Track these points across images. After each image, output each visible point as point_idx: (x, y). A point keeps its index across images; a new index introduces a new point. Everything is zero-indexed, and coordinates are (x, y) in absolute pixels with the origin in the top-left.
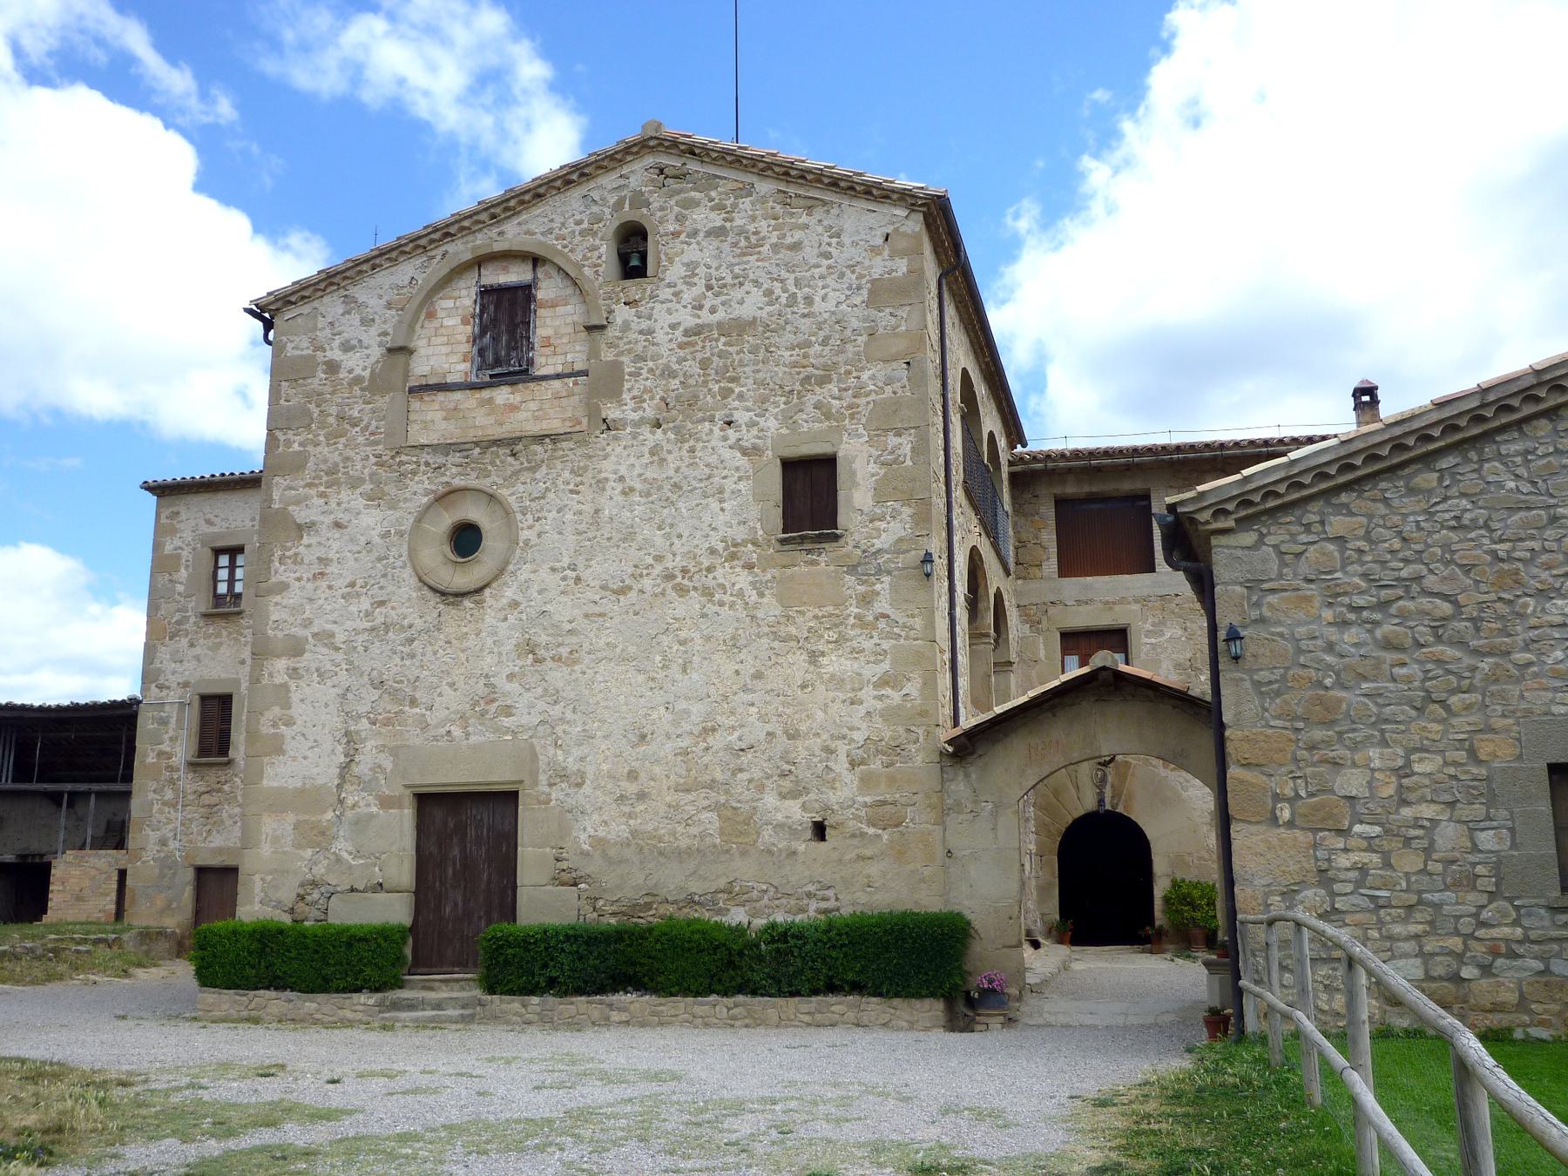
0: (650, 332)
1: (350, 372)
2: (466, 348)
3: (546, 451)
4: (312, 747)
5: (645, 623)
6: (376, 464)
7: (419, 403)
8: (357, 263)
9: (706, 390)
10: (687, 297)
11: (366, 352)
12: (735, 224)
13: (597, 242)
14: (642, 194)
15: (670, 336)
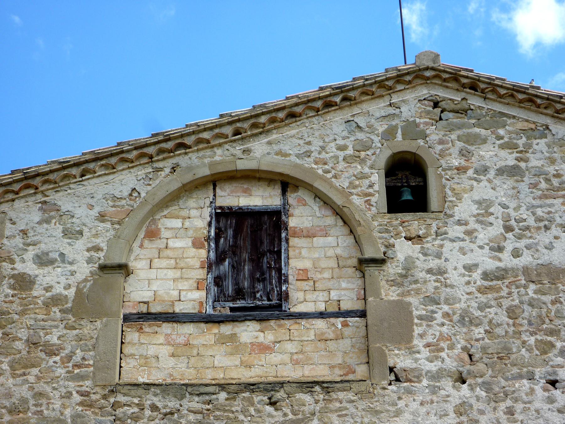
0: (441, 272)
1: (48, 289)
2: (201, 274)
3: (317, 402)
6: (81, 404)
7: (137, 334)
8: (65, 166)
9: (518, 342)
10: (483, 236)
11: (70, 268)
12: (530, 165)
13: (367, 170)
14: (417, 125)
15: (467, 278)
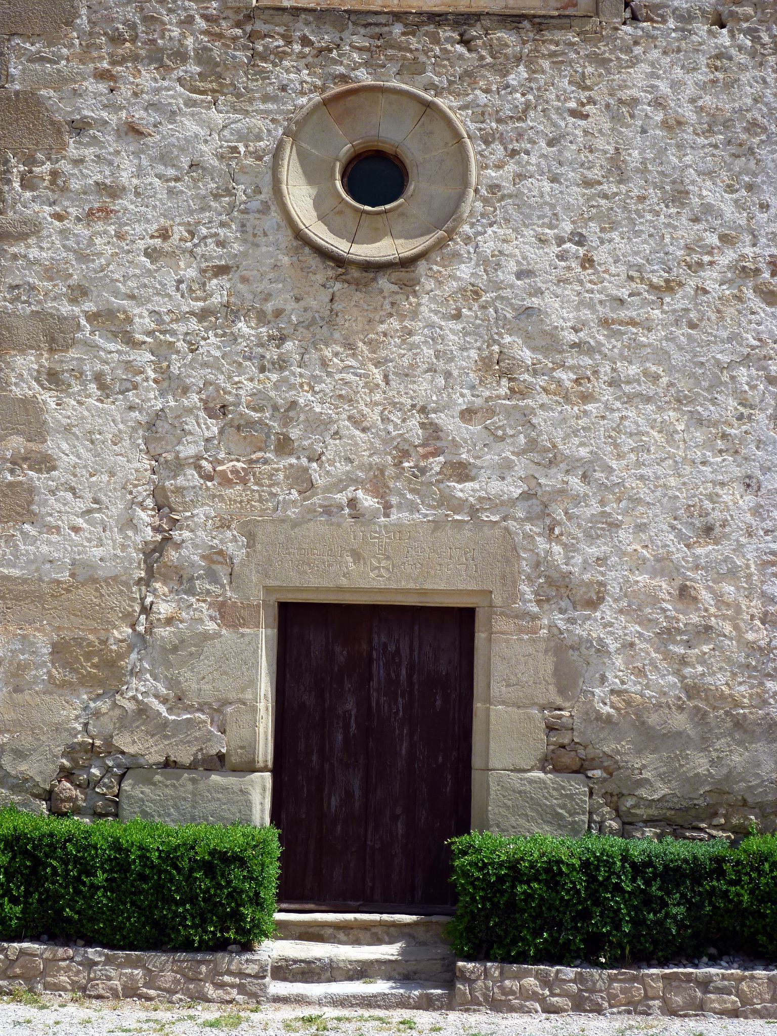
4: (89, 511)
5: (709, 343)
